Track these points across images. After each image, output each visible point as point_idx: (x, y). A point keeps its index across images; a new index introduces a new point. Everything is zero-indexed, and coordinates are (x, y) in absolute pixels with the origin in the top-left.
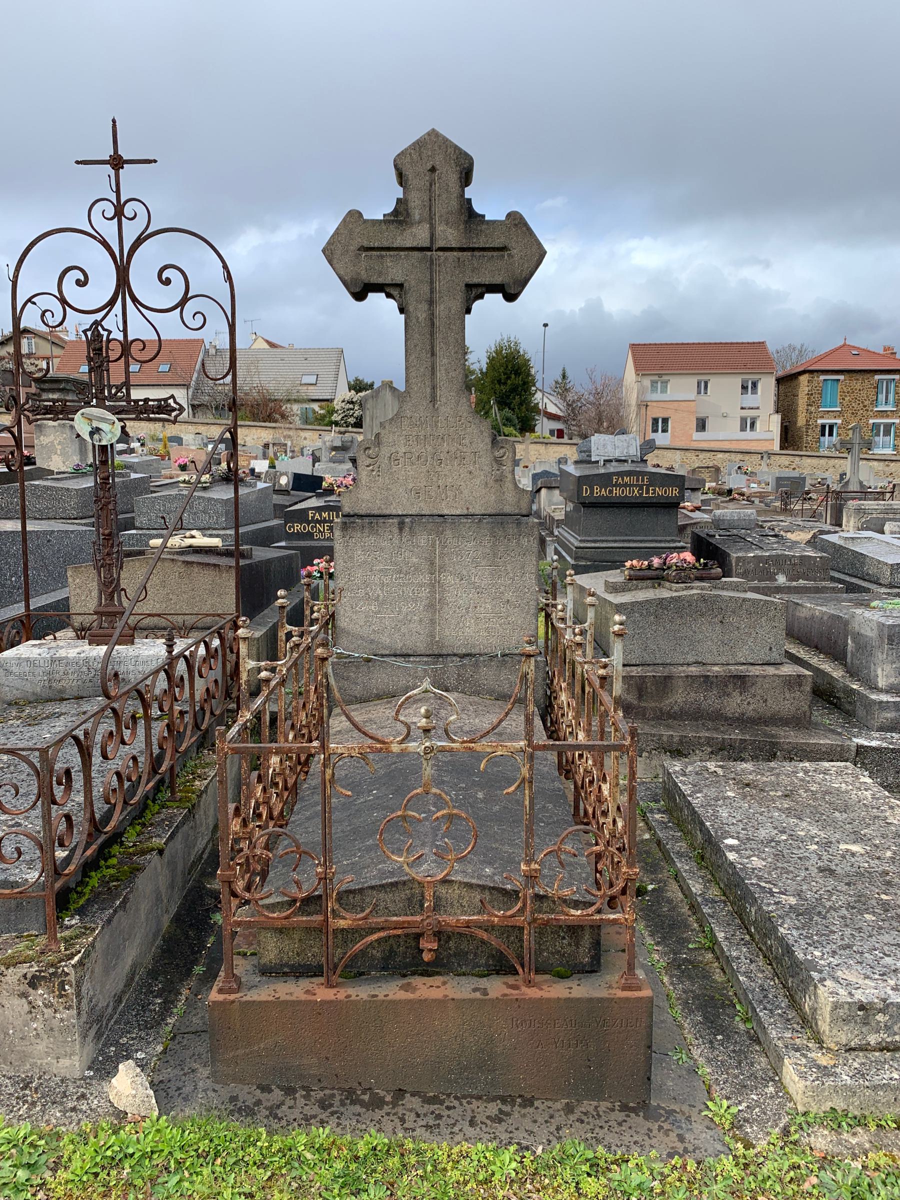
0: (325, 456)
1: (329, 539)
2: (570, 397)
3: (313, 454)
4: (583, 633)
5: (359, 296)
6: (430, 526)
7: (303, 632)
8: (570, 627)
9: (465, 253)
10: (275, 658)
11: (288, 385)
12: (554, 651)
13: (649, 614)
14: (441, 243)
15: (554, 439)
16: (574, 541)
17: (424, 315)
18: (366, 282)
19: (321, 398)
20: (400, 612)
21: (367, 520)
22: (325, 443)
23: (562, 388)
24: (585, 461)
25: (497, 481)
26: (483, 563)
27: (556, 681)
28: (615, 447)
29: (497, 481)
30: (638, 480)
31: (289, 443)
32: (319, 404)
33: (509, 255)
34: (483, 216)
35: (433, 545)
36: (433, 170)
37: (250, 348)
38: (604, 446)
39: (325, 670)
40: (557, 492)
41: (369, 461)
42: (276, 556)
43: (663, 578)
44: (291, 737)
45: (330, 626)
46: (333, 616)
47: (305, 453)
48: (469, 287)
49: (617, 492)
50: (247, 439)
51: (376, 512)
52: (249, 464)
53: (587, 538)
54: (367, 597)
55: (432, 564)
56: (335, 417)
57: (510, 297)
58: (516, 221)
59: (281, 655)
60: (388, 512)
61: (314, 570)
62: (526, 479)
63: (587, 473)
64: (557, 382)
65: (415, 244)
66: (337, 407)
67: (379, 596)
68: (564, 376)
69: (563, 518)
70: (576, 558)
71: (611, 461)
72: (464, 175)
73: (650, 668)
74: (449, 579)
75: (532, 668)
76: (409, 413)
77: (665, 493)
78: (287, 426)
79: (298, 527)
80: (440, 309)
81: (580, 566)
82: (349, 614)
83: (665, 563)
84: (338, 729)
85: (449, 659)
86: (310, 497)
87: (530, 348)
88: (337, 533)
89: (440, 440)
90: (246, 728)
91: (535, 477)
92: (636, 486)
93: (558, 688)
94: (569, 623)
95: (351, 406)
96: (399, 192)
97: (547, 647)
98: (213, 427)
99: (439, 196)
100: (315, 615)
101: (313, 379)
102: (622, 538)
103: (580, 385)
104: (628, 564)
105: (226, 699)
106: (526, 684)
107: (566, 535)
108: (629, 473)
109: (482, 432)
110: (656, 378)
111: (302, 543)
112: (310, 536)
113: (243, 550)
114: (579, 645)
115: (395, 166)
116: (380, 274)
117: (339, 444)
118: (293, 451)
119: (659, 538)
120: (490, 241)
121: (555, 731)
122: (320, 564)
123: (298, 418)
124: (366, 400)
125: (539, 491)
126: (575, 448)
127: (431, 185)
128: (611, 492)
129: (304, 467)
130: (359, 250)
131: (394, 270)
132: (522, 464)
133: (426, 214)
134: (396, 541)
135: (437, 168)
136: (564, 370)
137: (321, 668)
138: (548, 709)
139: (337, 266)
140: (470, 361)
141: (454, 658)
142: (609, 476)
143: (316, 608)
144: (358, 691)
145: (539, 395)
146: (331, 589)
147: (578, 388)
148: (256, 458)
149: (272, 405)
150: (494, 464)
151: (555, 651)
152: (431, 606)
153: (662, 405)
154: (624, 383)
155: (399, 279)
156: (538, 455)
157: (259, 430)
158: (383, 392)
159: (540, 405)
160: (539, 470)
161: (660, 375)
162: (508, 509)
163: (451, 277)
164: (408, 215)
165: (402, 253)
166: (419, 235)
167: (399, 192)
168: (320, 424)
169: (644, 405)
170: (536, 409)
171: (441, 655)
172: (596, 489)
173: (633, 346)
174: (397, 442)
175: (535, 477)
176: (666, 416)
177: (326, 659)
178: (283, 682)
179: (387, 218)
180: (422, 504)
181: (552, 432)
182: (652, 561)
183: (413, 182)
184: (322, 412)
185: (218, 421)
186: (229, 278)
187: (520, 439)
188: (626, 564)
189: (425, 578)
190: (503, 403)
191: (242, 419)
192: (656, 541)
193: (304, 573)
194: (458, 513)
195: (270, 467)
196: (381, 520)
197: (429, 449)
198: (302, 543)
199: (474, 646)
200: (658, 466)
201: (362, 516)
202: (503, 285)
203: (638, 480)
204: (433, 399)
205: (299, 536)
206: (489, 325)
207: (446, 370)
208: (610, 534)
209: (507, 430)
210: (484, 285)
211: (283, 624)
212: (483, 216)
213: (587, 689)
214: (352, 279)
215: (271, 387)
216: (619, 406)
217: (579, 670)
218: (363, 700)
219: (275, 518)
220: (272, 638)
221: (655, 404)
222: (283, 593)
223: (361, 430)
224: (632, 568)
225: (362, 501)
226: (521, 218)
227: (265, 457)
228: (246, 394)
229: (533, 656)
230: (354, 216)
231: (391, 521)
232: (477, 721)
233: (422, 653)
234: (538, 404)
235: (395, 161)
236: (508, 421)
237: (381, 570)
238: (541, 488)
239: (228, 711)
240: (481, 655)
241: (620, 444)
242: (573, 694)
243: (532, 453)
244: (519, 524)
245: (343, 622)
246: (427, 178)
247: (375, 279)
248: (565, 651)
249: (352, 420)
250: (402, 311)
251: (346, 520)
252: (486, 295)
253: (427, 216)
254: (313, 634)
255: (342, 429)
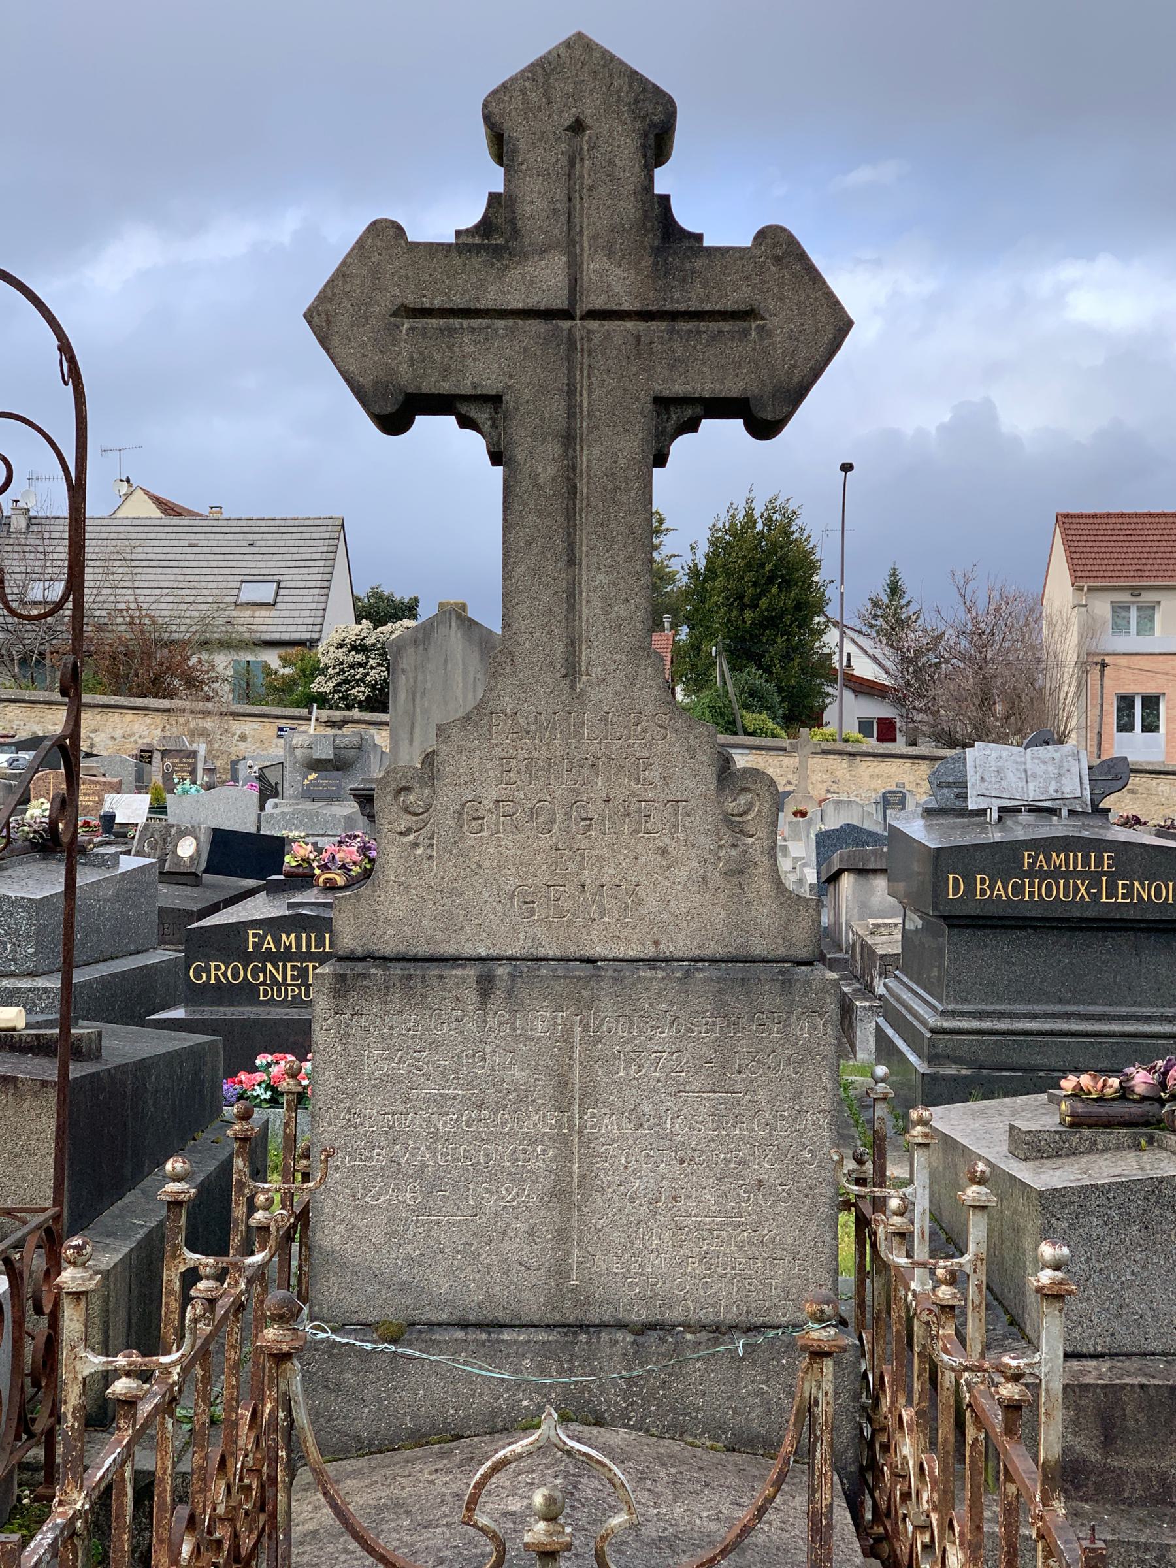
0: (291, 782)
1: (297, 1002)
2: (911, 639)
3: (261, 777)
4: (954, 1279)
5: (394, 422)
6: (558, 987)
7: (225, 1271)
8: (924, 1265)
9: (654, 325)
10: (151, 1345)
11: (204, 606)
12: (872, 1300)
13: (1127, 1219)
14: (597, 302)
15: (871, 744)
16: (926, 1012)
17: (552, 470)
18: (411, 389)
19: (286, 637)
20: (477, 1210)
21: (397, 970)
22: (291, 749)
23: (891, 616)
24: (951, 807)
25: (730, 873)
26: (696, 1084)
27: (886, 1403)
28: (1027, 776)
29: (730, 873)
30: (1086, 862)
31: (202, 749)
32: (282, 651)
33: (761, 330)
34: (699, 237)
35: (567, 1037)
36: (578, 127)
37: (112, 517)
38: (999, 772)
39: (283, 1387)
40: (880, 884)
41: (405, 821)
42: (161, 1050)
43: (1159, 1123)
44: (186, 1550)
45: (295, 1247)
46: (303, 1217)
47: (243, 772)
48: (663, 403)
49: (1034, 890)
50: (98, 738)
51: (422, 950)
52: (101, 802)
53: (959, 1007)
54: (395, 1172)
55: (564, 1083)
56: (321, 685)
57: (764, 428)
58: (779, 249)
59: (168, 1331)
60: (450, 950)
61: (254, 1083)
62: (801, 845)
63: (957, 840)
64: (875, 604)
65: (531, 303)
66: (325, 660)
67: (424, 1165)
68: (895, 589)
69: (898, 950)
70: (932, 1059)
71: (1016, 810)
72: (651, 141)
73: (1133, 1364)
74: (607, 1125)
75: (828, 1386)
76: (509, 704)
77: (1158, 894)
78: (200, 705)
79: (218, 971)
80: (591, 456)
81: (944, 1078)
82: (346, 1213)
83: (1163, 1085)
84: (310, 1527)
85: (605, 1336)
86: (252, 892)
87: (815, 527)
88: (322, 1003)
89: (586, 771)
90: (74, 1534)
91: (826, 842)
92: (1083, 876)
93: (891, 1422)
94: (921, 1251)
95: (360, 657)
96: (495, 179)
97: (861, 1305)
98: (12, 708)
99: (591, 188)
100: (259, 1216)
101: (266, 592)
102: (1050, 1008)
103: (936, 608)
104: (1069, 1083)
105: (18, 1438)
106: (812, 1428)
107: (906, 996)
108: (1065, 844)
109: (693, 752)
110: (1125, 597)
111: (228, 1012)
112: (247, 993)
113: (80, 1038)
114: (947, 1309)
115: (487, 118)
116: (445, 372)
117: (326, 752)
118: (210, 770)
119: (1147, 1011)
120: (713, 298)
121: (886, 1537)
122: (275, 1066)
123: (227, 687)
124: (399, 651)
125: (834, 878)
126: (924, 769)
127: (572, 164)
128: (1018, 889)
129: (236, 810)
130: (395, 314)
131: (481, 364)
132: (790, 807)
133: (559, 231)
134: (471, 1026)
135: (587, 125)
136: (894, 574)
137: (274, 1382)
138: (864, 1474)
139: (339, 351)
140: (665, 550)
141: (619, 1335)
142: (1014, 848)
143: (261, 1199)
144: (363, 1420)
145: (832, 637)
146: (301, 1145)
147: (929, 620)
148: (117, 789)
149: (161, 654)
150: (724, 829)
151: (881, 1318)
152: (558, 1194)
153: (1142, 663)
154: (1046, 610)
155: (490, 386)
156: (834, 782)
157: (129, 716)
158: (443, 630)
159: (836, 658)
160: (833, 823)
161: (1135, 591)
162: (759, 946)
163: (617, 378)
164: (516, 232)
165: (500, 323)
166: (541, 280)
167: (495, 179)
168: (280, 703)
169: (1095, 663)
170: (824, 670)
171: (583, 1327)
172: (981, 882)
173: (1066, 520)
174: (479, 776)
175: (826, 842)
176: (1151, 689)
177: (287, 1356)
178: (170, 1404)
179: (464, 239)
180: (540, 932)
181: (865, 726)
182: (1130, 1078)
183: (530, 156)
184: (287, 671)
185: (27, 694)
186: (73, 376)
187: (786, 742)
188: (1063, 1083)
189: (545, 1122)
190: (743, 651)
191: (93, 691)
192: (1138, 1018)
193: (228, 1089)
194: (631, 953)
195: (152, 810)
196: (434, 971)
197: (560, 791)
198: (228, 1012)
199: (670, 1304)
200: (1138, 821)
201: (385, 959)
202: (747, 400)
203: (1086, 862)
204: (572, 670)
205: (221, 993)
206: (707, 483)
207: (603, 599)
208: (1019, 996)
209: (751, 719)
210: (700, 400)
211: (176, 1247)
212: (699, 237)
213: (971, 1432)
214: (376, 382)
215: (163, 610)
216: (1036, 663)
217: (947, 1379)
218: (376, 1447)
219: (162, 942)
220: (141, 1279)
221: (1123, 661)
222: (179, 1166)
223: (384, 717)
224: (1078, 1094)
225: (387, 920)
226: (792, 242)
227: (141, 786)
228: (100, 628)
229: (828, 1354)
230: (386, 232)
231: (458, 972)
232: (678, 1509)
233: (535, 1319)
234: (829, 656)
235: (485, 105)
236: (754, 698)
237: (432, 1100)
238: (839, 873)
239: (23, 1466)
240: (688, 1327)
241: (1040, 769)
242: (933, 1444)
243: (816, 777)
244: (787, 983)
245: (329, 1234)
246: (563, 147)
247: (433, 384)
248: (910, 1320)
249: (360, 692)
250: (496, 458)
251: (345, 968)
252: (705, 423)
253: (562, 238)
254: (249, 1273)
255: (337, 715)
